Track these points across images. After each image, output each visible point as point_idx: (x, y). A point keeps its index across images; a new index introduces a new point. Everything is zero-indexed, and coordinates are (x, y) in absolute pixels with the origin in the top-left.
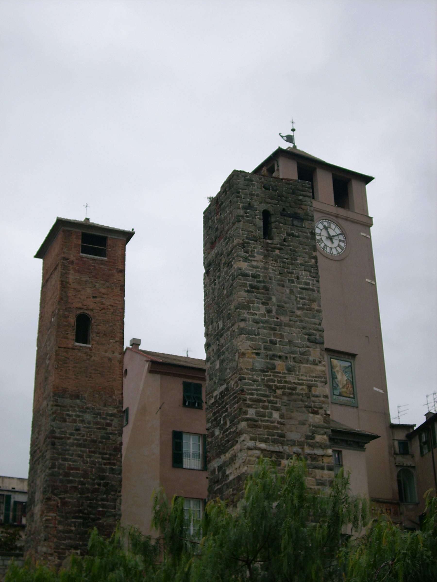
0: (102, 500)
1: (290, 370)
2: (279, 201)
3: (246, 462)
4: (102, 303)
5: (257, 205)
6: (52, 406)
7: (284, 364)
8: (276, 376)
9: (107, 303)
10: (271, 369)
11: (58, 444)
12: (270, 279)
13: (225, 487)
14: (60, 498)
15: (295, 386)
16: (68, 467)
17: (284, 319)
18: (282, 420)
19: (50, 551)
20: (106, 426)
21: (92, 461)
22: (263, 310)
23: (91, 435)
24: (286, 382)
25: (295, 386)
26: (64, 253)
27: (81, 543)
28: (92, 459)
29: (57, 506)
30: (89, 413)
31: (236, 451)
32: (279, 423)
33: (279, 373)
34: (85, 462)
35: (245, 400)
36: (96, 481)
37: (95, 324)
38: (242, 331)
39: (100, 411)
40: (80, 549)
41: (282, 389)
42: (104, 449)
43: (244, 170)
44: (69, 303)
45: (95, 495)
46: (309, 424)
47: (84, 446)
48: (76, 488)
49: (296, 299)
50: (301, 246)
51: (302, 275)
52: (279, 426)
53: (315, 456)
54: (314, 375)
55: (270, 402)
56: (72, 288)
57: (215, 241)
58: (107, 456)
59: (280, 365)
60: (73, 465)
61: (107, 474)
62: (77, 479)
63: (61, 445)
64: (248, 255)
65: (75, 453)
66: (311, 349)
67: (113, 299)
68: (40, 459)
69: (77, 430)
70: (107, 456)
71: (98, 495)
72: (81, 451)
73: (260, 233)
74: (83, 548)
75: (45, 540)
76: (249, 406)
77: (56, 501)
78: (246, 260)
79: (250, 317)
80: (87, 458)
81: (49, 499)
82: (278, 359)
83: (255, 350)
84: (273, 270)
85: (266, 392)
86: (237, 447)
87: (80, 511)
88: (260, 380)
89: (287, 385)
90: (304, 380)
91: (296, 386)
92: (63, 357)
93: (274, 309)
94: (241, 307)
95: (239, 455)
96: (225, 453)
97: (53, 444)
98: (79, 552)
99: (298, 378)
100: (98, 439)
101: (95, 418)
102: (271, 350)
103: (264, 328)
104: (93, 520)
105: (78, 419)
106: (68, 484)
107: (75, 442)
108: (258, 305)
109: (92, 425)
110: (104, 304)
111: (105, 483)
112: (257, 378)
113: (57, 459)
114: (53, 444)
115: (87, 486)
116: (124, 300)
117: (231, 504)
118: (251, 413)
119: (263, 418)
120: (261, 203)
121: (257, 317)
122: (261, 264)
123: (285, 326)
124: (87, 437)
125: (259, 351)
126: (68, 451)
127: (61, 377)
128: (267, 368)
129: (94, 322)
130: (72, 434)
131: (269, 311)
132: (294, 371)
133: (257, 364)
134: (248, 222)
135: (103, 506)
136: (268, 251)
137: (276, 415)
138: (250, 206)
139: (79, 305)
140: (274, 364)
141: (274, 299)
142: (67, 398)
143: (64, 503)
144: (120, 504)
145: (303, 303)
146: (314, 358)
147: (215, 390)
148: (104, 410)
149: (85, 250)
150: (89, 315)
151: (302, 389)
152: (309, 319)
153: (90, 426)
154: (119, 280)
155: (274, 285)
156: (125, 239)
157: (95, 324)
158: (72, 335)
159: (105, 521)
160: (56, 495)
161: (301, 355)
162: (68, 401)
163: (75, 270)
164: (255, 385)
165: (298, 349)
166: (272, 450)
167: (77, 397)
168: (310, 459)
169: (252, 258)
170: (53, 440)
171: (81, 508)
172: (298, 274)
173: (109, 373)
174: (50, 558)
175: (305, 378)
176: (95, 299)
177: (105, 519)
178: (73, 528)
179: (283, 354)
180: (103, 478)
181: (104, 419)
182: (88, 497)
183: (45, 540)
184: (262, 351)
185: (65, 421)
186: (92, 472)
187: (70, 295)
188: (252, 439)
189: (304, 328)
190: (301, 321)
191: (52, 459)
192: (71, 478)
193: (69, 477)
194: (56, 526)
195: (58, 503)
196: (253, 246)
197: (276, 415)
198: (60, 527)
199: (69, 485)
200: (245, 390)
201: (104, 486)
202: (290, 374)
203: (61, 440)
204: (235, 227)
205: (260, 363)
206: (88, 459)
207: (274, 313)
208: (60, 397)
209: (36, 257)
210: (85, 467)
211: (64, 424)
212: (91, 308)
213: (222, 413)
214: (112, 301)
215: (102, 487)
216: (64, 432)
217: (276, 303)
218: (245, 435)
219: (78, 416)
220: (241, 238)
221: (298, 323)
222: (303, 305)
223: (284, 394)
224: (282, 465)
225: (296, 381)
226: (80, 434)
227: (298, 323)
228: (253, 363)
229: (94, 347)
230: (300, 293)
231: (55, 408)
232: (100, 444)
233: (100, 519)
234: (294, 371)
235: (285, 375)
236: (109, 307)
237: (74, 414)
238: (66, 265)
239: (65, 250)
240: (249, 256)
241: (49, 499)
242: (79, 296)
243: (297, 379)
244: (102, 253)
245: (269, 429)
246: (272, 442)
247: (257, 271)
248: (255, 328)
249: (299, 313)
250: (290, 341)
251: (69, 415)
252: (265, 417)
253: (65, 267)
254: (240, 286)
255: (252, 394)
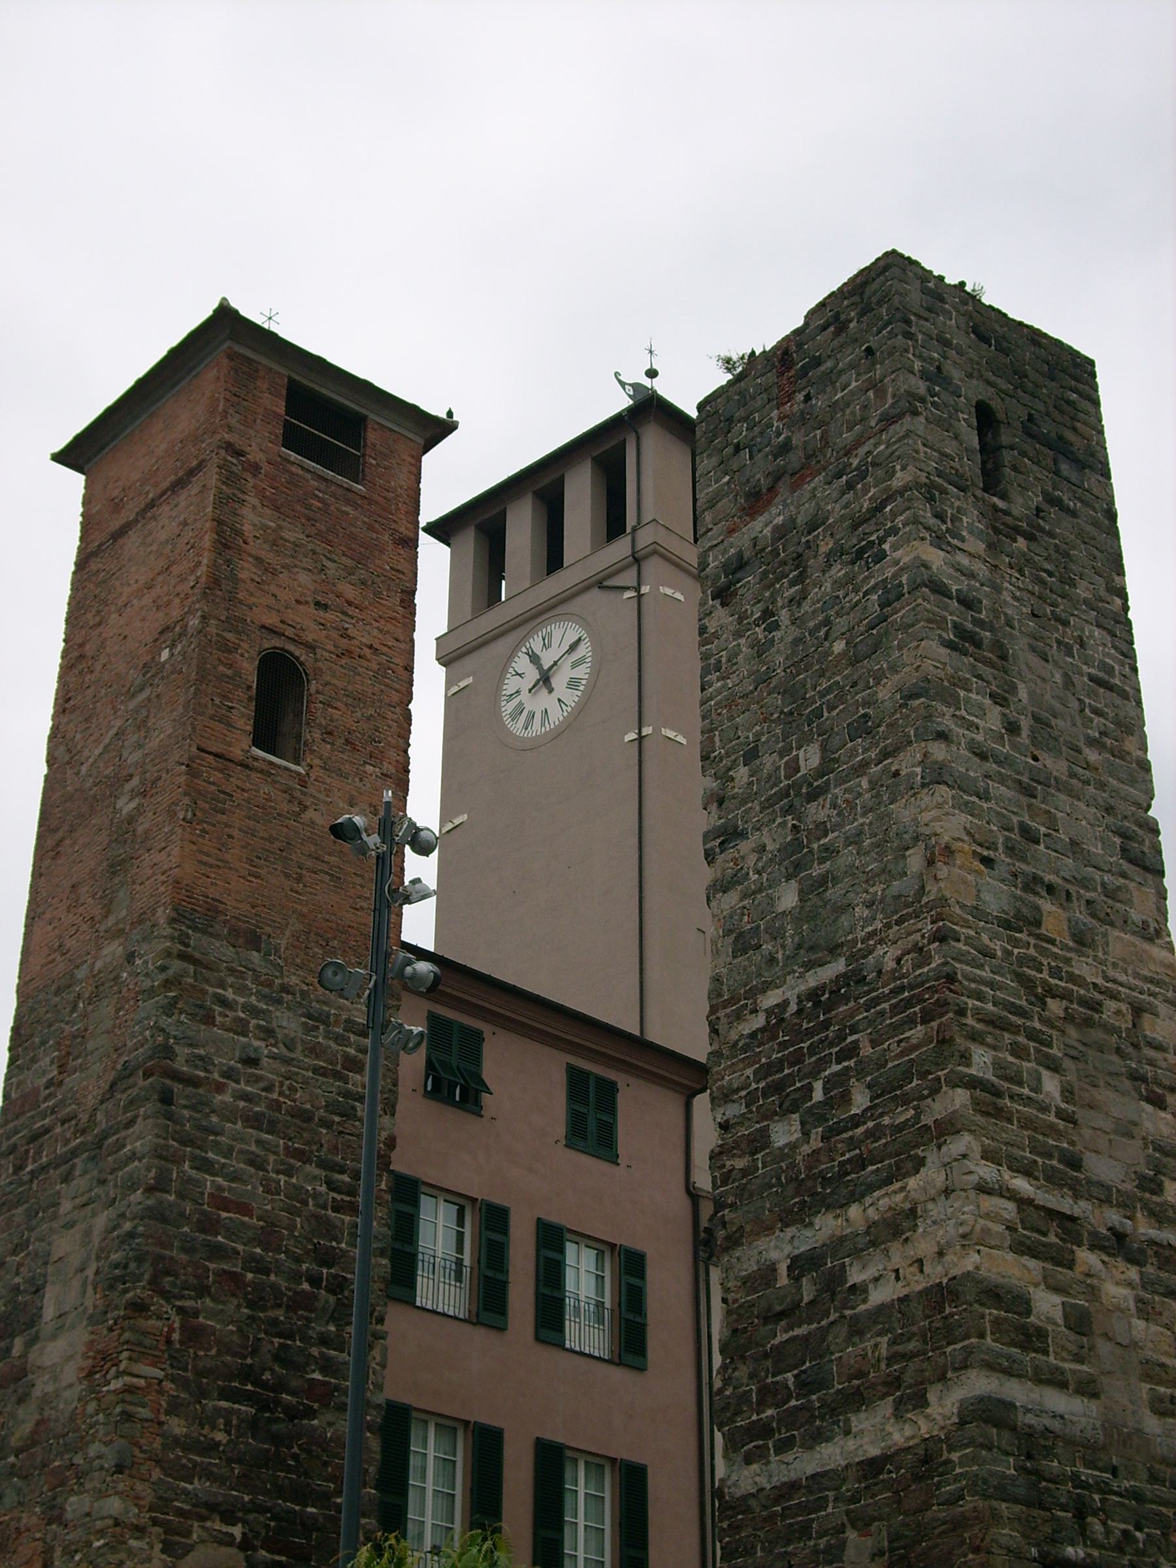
0: (324, 1340)
1: (1082, 940)
2: (1016, 388)
3: (975, 1237)
4: (345, 635)
5: (960, 380)
6: (168, 954)
7: (1064, 915)
8: (1042, 951)
9: (363, 635)
10: (1030, 923)
11: (183, 1102)
12: (1009, 623)
13: (843, 1331)
14: (181, 1310)
15: (1098, 996)
16: (211, 1195)
17: (1055, 765)
18: (1071, 1108)
19: (133, 1515)
20: (344, 1068)
21: (294, 1185)
22: (993, 719)
23: (292, 1089)
24: (1072, 978)
25: (1098, 996)
26: (230, 428)
27: (247, 1498)
28: (294, 1180)
29: (169, 1342)
30: (289, 1008)
31: (913, 1194)
32: (1060, 1114)
33: (1052, 942)
34: (270, 1189)
35: (961, 1012)
36: (304, 1266)
37: (321, 698)
38: (937, 775)
39: (326, 1009)
40: (245, 1522)
41: (1062, 998)
42: (335, 1149)
43: (919, 260)
44: (241, 602)
45: (301, 1318)
46: (1144, 1138)
47: (272, 1128)
48: (234, 1277)
49: (1082, 711)
50: (1083, 546)
51: (1091, 636)
52: (1061, 1124)
53: (1167, 1253)
54: (1146, 972)
55: (1032, 1035)
56: (250, 555)
57: (771, 489)
58: (345, 1178)
59: (1055, 919)
60: (230, 1189)
61: (343, 1245)
62: (240, 1247)
63: (192, 1107)
64: (944, 527)
65: (238, 1146)
66: (1132, 885)
67: (381, 631)
68: (79, 1162)
69: (251, 1061)
70: (345, 1178)
71: (308, 1319)
72: (259, 1142)
73: (971, 468)
74: (251, 1517)
75: (119, 1469)
76: (974, 1037)
77: (165, 1320)
78: (939, 541)
79: (961, 731)
80: (278, 1172)
81: (139, 1308)
82: (1044, 893)
83: (981, 845)
84: (1014, 598)
85: (1020, 998)
86: (931, 1176)
87: (247, 1374)
88: (999, 953)
89: (1075, 988)
90: (1121, 985)
91: (1101, 997)
92: (213, 788)
93: (1025, 723)
94: (932, 692)
95: (935, 1210)
96: (844, 1206)
97: (167, 1098)
98: (237, 1531)
99: (1103, 971)
100: (318, 1109)
101: (308, 1029)
102: (1023, 859)
103: (1002, 780)
104: (293, 1414)
105: (254, 1022)
106: (209, 1259)
107: (242, 1104)
108: (979, 697)
109: (297, 1054)
110: (351, 638)
111: (336, 1276)
112: (992, 945)
113: (178, 1161)
114: (167, 1098)
115: (273, 1277)
116: (412, 641)
117: (884, 1396)
118: (981, 1062)
119: (1016, 1089)
120: (970, 376)
121: (980, 738)
122: (981, 569)
123: (1059, 790)
124: (281, 1094)
125: (992, 854)
126: (217, 1134)
127: (205, 858)
128: (1018, 915)
129: (318, 692)
130: (230, 1074)
131: (1013, 728)
132: (1092, 945)
133: (987, 897)
134: (939, 422)
135: (327, 1366)
136: (1001, 530)
137: (1051, 1085)
138: (936, 376)
139: (272, 620)
140: (1037, 909)
141: (1023, 693)
142: (217, 936)
143: (194, 1335)
144: (384, 1366)
145: (1103, 729)
146: (1144, 918)
147: (766, 987)
148: (340, 1008)
149: (292, 438)
150: (302, 664)
151: (1118, 1012)
152: (1121, 785)
153: (293, 1055)
154: (398, 571)
155: (1018, 647)
156: (421, 441)
157: (321, 698)
158: (243, 718)
159: (330, 1424)
160: (166, 1295)
161: (1106, 896)
162: (221, 951)
163: (261, 494)
164: (987, 968)
165: (1097, 876)
166: (1049, 1205)
167: (254, 941)
168: (1154, 1260)
169: (955, 542)
170: (168, 1082)
171: (249, 1361)
172: (1083, 630)
173: (358, 880)
174: (133, 1543)
175: (1122, 978)
176: (322, 613)
177: (330, 1417)
178: (220, 1437)
179: (1060, 881)
180: (327, 1258)
181: (338, 1039)
182: (274, 1322)
183: (119, 1469)
184: (1000, 855)
185: (209, 1020)
186: (291, 1228)
187: (244, 575)
188: (988, 1155)
189: (1109, 809)
190: (1102, 786)
191: (159, 1153)
192: (220, 1238)
193: (217, 1234)
194: (163, 1418)
195: (171, 1330)
196: (957, 503)
197: (1051, 1085)
198: (177, 1426)
199: (212, 1266)
200: (959, 977)
201: (331, 1291)
202: (1083, 954)
203: (190, 1090)
204: (898, 429)
205: (996, 896)
206: (282, 1178)
207: (1024, 737)
208: (195, 929)
209: (62, 458)
210: (269, 1207)
211: (203, 1031)
212: (309, 637)
213: (824, 1062)
214: (375, 632)
215: (323, 1292)
216: (205, 1062)
217: (1031, 709)
218: (967, 1137)
219: (255, 1012)
220: (923, 466)
221: (1091, 789)
222: (1100, 733)
223: (1069, 1018)
224: (1079, 1269)
225: (1099, 981)
226: (259, 1079)
227: (1091, 789)
228: (979, 891)
229: (313, 776)
230: (1092, 694)
231: (177, 965)
232: (324, 1131)
233: (310, 1413)
234: (1092, 945)
235: (1069, 955)
236: (367, 651)
237: (242, 1000)
238: (234, 469)
239: (234, 420)
240: (948, 530)
241: (139, 1308)
242: (273, 589)
243: (1100, 974)
244: (351, 467)
245: (1035, 1130)
246: (1048, 1179)
247: (970, 587)
248: (975, 771)
249: (1092, 756)
250: (1073, 843)
251: (223, 1002)
252: (1020, 1084)
253: (229, 478)
254: (929, 621)
255: (980, 997)
